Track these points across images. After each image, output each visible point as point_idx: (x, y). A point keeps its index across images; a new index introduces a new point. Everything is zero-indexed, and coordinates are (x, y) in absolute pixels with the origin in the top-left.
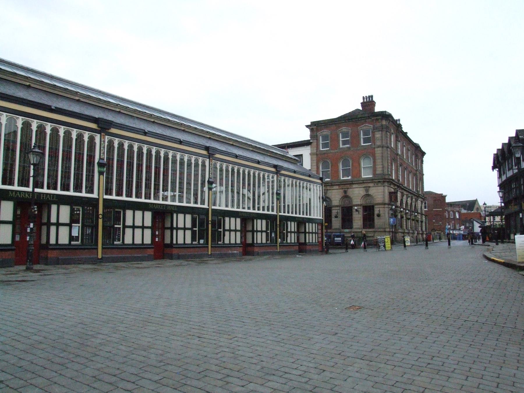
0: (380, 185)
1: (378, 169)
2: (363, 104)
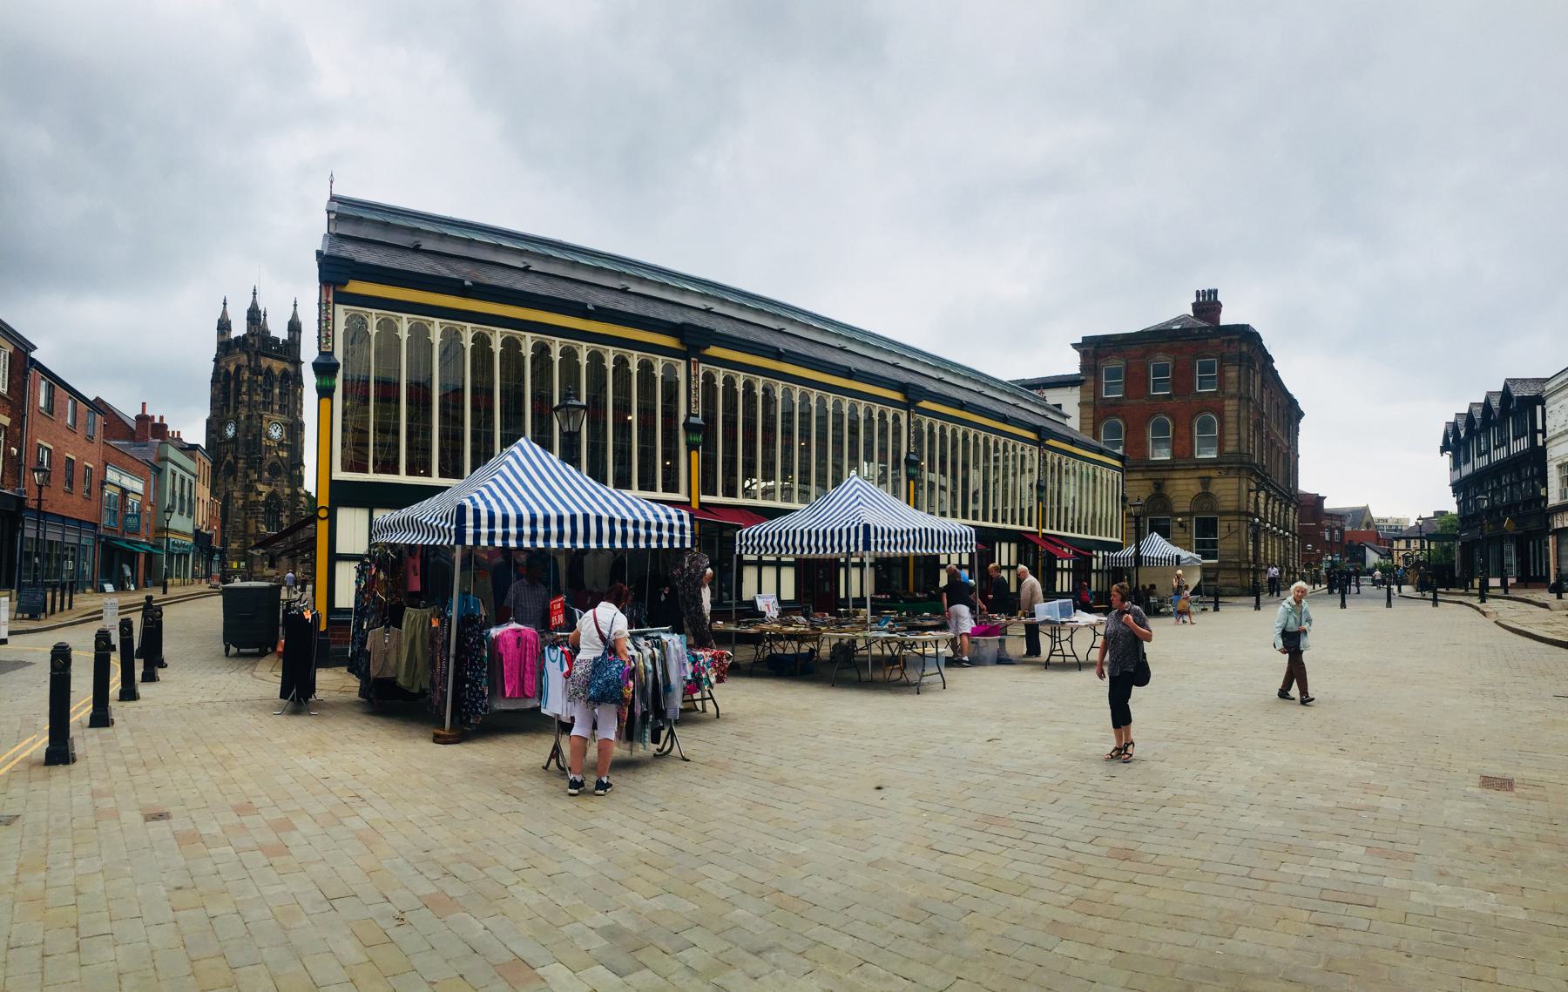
0: (1232, 473)
1: (1229, 443)
2: (1196, 306)
